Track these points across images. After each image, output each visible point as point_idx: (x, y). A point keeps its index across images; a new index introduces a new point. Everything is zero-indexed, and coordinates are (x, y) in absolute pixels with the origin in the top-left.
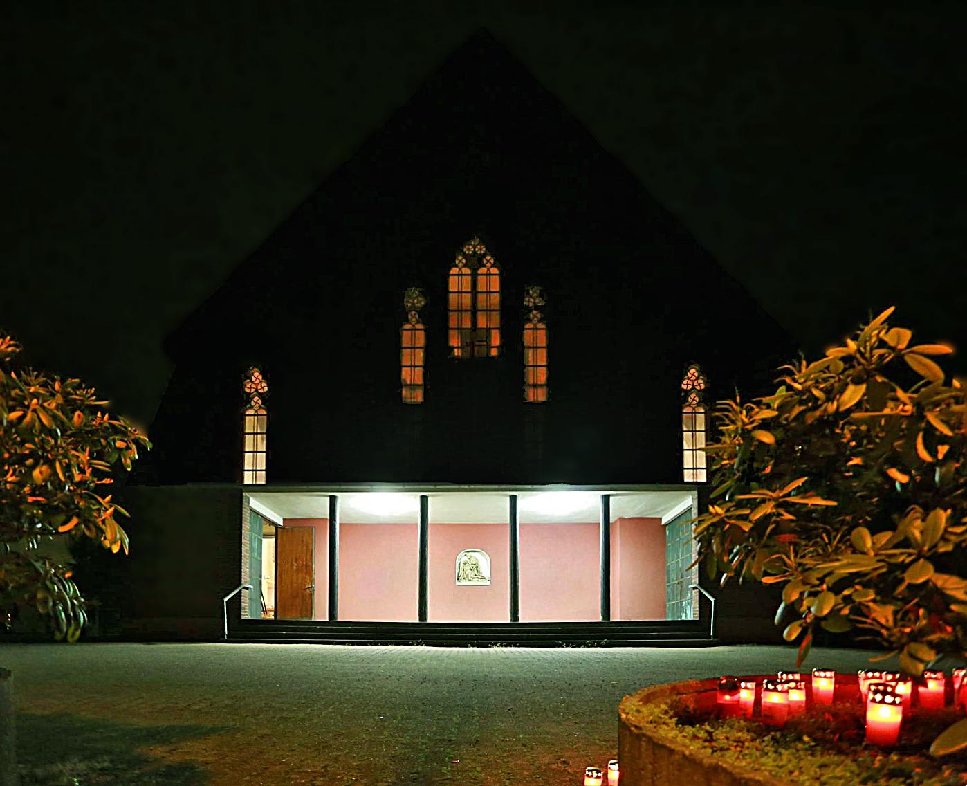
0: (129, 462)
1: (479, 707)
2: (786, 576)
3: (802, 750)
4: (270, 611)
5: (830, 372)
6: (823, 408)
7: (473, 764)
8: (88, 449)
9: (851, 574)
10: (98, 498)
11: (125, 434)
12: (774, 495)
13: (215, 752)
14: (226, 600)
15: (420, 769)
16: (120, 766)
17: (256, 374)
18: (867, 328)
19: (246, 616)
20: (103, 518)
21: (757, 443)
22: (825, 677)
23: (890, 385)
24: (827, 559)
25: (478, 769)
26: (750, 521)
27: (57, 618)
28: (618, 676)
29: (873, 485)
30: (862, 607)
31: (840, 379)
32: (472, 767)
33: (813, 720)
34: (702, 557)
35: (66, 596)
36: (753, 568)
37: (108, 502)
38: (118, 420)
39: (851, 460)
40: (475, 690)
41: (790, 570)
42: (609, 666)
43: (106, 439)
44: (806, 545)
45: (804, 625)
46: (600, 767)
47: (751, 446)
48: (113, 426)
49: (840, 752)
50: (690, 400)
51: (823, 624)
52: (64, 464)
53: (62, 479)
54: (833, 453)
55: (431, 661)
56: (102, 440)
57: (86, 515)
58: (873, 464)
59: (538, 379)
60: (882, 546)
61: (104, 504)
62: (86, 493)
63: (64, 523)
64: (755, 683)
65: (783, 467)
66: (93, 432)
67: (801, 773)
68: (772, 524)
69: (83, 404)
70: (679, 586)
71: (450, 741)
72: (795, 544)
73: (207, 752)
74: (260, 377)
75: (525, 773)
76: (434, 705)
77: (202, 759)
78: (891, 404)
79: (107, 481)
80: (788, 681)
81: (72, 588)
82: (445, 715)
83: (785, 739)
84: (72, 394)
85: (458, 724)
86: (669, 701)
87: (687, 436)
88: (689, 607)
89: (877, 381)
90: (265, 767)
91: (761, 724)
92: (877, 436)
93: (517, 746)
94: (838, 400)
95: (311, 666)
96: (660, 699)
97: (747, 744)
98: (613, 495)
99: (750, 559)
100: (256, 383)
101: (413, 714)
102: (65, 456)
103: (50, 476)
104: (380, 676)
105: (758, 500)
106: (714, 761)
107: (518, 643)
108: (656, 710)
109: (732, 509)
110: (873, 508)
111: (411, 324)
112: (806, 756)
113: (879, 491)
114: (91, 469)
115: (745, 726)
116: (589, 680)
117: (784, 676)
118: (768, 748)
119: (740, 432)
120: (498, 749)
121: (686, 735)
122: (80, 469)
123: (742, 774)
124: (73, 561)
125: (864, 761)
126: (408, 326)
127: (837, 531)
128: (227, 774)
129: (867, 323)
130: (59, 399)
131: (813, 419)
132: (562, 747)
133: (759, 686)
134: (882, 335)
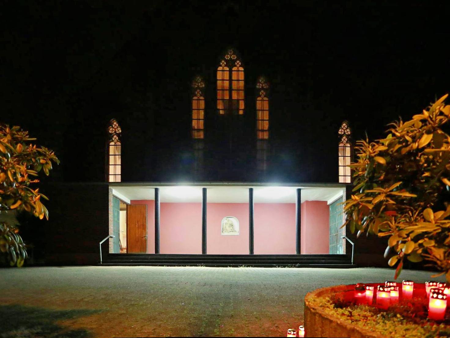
0: (47, 171)
1: (233, 298)
2: (390, 233)
3: (396, 321)
4: (124, 249)
5: (414, 127)
6: (410, 146)
7: (231, 327)
8: (25, 164)
9: (423, 232)
10: (31, 190)
11: (45, 155)
12: (385, 190)
13: (96, 323)
14: (101, 243)
15: (203, 330)
16: (46, 331)
17: (115, 123)
18: (434, 105)
19: (112, 251)
20: (34, 200)
21: (376, 163)
22: (409, 285)
23: (445, 135)
24: (411, 225)
25: (233, 330)
26: (373, 204)
27: (11, 254)
28: (305, 283)
29: (435, 187)
30: (428, 250)
31: (419, 131)
32: (230, 329)
33: (402, 306)
34: (348, 222)
35: (16, 243)
36: (374, 228)
37: (37, 192)
38: (41, 148)
39: (424, 173)
40: (231, 290)
41: (392, 230)
42: (300, 277)
43: (35, 158)
44: (400, 217)
45: (399, 258)
46: (295, 329)
47: (374, 164)
48: (39, 152)
49: (415, 323)
50: (343, 140)
51: (409, 258)
52: (13, 172)
53: (11, 179)
54: (415, 169)
55: (209, 274)
56: (33, 159)
57: (25, 199)
58: (435, 176)
59: (264, 127)
60: (439, 219)
61: (34, 193)
62: (24, 187)
63: (14, 204)
64: (373, 287)
65: (390, 176)
66: (28, 155)
67: (396, 333)
68: (384, 206)
69: (22, 140)
70: (336, 236)
71: (218, 316)
72: (395, 216)
73: (92, 323)
74: (117, 125)
75: (257, 332)
76: (210, 297)
77: (90, 327)
78: (445, 145)
79: (36, 181)
80: (390, 287)
81: (19, 238)
82: (216, 302)
83: (388, 316)
84: (16, 135)
85: (223, 307)
86: (330, 296)
87: (341, 159)
88: (341, 247)
89: (438, 133)
90: (123, 330)
91: (376, 308)
92: (438, 162)
93: (253, 318)
94: (418, 142)
95: (146, 277)
96: (326, 295)
97: (369, 318)
98: (302, 189)
99: (372, 223)
100: (115, 128)
101: (199, 302)
102: (13, 168)
103: (5, 179)
104: (182, 282)
105: (377, 193)
106: (352, 327)
107: (253, 265)
108: (324, 300)
109: (363, 197)
110: (434, 199)
111: (197, 96)
112: (398, 324)
113: (438, 189)
114: (27, 175)
115: (368, 309)
116: (289, 284)
117: (388, 284)
118: (380, 320)
119: (368, 157)
120: (243, 320)
121: (338, 313)
122: (21, 175)
123: (367, 333)
124: (18, 224)
125: (427, 328)
126: (195, 98)
127: (416, 210)
128: (102, 334)
129: (434, 102)
130: (9, 137)
131: (405, 152)
132: (276, 319)
133: (375, 289)
134: (441, 108)
